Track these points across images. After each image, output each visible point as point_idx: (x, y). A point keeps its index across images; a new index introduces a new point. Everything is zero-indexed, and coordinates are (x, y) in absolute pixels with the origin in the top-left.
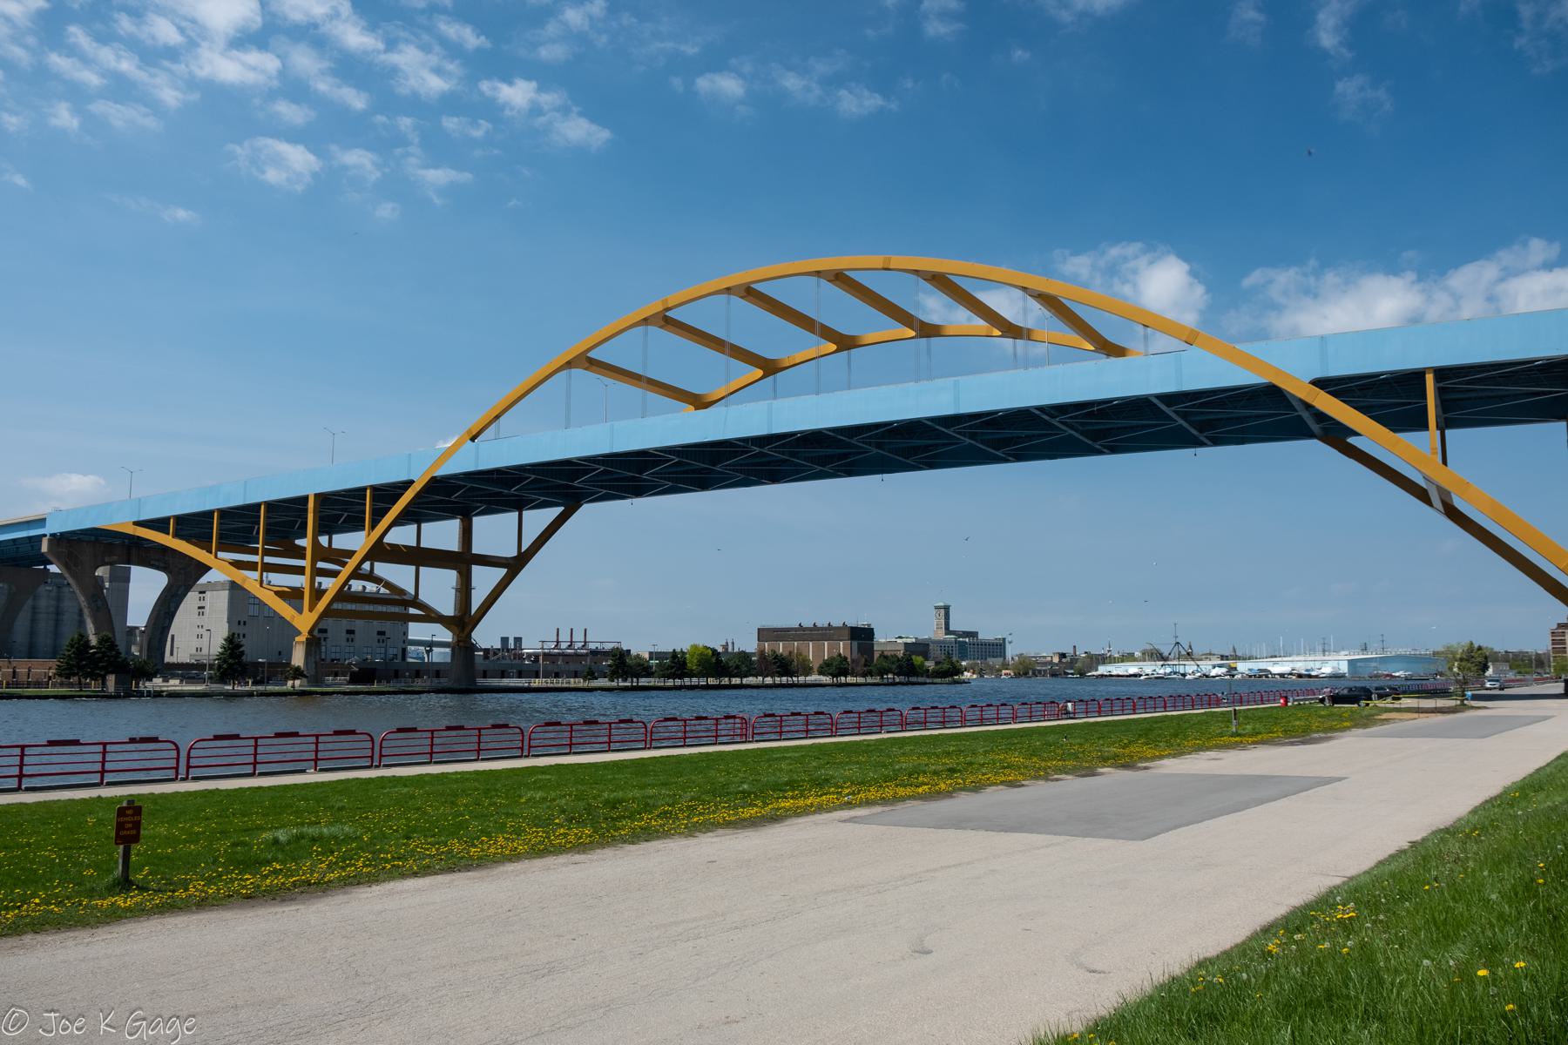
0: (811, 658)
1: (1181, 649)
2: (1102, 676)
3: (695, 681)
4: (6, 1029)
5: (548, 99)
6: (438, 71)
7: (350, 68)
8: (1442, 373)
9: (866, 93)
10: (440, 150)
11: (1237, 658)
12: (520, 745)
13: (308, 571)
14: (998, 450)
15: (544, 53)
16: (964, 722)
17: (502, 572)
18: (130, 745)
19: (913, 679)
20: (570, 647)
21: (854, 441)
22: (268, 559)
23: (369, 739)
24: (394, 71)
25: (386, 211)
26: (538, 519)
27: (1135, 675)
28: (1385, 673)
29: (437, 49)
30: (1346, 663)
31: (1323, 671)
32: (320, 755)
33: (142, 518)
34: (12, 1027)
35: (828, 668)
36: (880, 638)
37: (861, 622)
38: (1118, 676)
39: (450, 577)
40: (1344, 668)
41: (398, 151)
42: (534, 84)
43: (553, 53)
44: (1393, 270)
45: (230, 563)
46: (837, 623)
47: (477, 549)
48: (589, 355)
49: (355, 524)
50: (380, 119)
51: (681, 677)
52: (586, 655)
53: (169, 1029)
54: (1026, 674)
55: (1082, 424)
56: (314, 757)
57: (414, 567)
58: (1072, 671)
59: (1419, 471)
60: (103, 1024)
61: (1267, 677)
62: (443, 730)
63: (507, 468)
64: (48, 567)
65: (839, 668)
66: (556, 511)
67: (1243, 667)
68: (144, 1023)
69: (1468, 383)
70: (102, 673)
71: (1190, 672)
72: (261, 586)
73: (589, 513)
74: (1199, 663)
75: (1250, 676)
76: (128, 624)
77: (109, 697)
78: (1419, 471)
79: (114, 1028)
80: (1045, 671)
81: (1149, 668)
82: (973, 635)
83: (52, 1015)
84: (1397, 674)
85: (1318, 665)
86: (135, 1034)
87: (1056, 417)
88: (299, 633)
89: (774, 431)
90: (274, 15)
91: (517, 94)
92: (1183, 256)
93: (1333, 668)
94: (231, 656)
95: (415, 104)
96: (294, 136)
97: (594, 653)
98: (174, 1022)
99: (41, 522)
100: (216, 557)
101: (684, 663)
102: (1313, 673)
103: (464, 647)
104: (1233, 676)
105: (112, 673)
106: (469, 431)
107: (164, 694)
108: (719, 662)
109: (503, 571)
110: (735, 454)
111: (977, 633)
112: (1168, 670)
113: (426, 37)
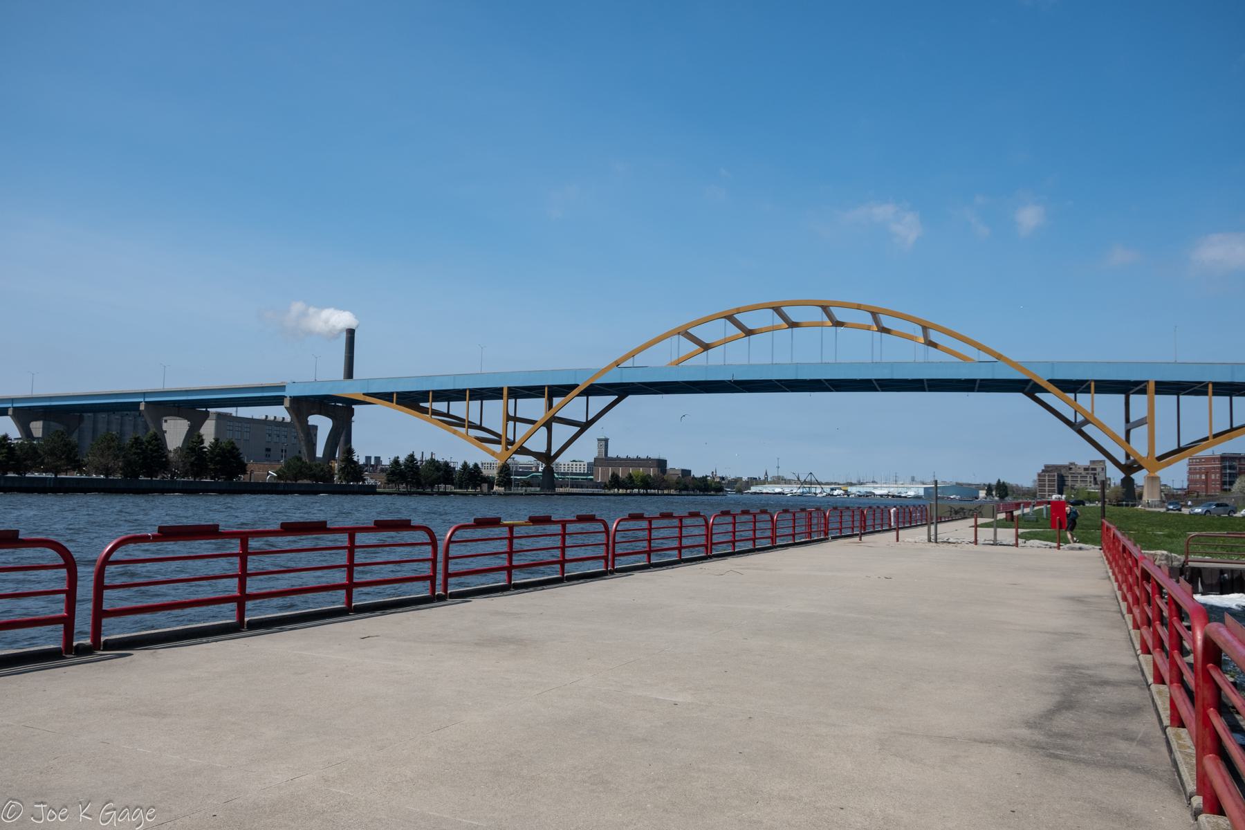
0: (620, 475)
1: (813, 478)
2: (755, 493)
4: (6, 818)
12: (57, 607)
17: (577, 429)
18: (722, 518)
23: (426, 538)
27: (779, 493)
31: (909, 493)
32: (570, 554)
33: (370, 392)
34: (10, 815)
36: (669, 466)
37: (662, 457)
38: (767, 493)
40: (921, 492)
60: (81, 814)
64: (208, 409)
68: (115, 812)
73: (631, 399)
74: (823, 486)
75: (860, 496)
79: (90, 816)
83: (42, 806)
84: (952, 497)
86: (107, 821)
89: (799, 378)
99: (282, 388)
101: (633, 481)
102: (903, 495)
103: (549, 471)
104: (848, 495)
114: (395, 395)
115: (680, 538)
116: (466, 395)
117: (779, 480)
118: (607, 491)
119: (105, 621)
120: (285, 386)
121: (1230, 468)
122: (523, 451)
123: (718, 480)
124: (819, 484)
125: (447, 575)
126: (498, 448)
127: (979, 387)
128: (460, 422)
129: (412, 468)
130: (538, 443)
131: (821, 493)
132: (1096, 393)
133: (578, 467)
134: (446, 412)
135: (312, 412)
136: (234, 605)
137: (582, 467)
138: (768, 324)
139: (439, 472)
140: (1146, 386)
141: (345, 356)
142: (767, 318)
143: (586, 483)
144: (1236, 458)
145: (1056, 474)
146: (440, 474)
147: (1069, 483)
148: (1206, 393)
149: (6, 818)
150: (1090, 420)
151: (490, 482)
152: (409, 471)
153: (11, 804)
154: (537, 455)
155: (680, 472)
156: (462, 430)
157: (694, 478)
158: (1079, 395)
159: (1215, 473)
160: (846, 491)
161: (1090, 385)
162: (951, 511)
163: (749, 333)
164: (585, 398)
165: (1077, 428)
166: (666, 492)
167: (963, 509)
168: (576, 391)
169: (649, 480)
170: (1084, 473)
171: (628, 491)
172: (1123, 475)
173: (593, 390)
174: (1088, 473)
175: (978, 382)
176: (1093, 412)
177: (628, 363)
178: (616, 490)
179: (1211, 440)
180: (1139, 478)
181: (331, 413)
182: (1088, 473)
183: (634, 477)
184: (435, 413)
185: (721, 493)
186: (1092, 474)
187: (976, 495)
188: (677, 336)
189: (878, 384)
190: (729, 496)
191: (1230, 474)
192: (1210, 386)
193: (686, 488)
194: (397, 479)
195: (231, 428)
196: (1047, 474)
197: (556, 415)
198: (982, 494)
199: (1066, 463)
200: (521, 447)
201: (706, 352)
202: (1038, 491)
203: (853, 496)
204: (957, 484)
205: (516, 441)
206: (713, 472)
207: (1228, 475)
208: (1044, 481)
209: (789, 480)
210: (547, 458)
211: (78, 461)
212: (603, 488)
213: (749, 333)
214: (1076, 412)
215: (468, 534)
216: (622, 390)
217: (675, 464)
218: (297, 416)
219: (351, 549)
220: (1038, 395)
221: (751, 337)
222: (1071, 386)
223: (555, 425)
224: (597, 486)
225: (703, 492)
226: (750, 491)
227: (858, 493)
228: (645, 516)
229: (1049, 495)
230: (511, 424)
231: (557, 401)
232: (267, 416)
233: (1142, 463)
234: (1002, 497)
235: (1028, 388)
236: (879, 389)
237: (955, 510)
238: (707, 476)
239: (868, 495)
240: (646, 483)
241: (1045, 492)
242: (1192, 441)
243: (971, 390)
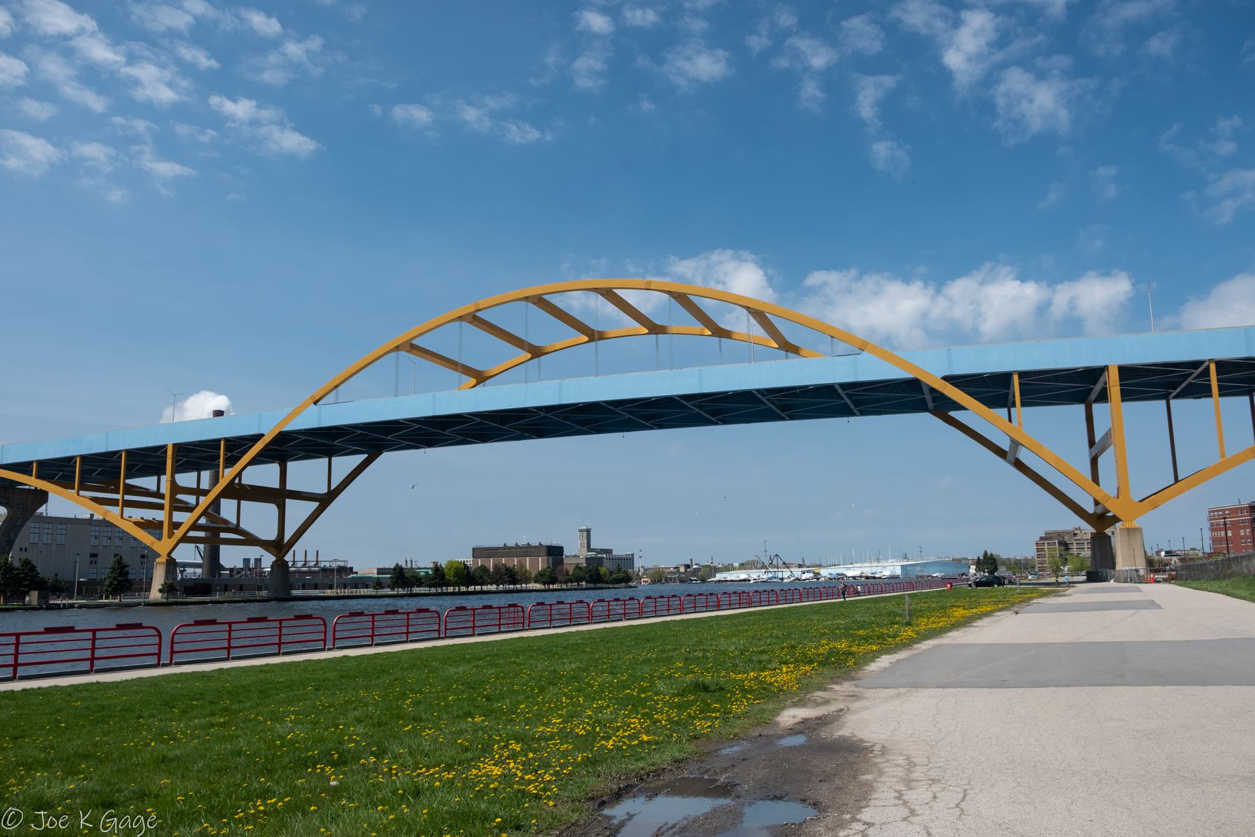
2: (719, 581)
3: (451, 589)
5: (267, 114)
6: (170, 85)
7: (92, 76)
8: (1022, 375)
9: (528, 129)
10: (168, 148)
11: (820, 566)
12: (155, 649)
13: (167, 507)
14: (713, 417)
15: (269, 77)
16: (590, 619)
17: (315, 505)
19: (599, 585)
20: (304, 565)
21: (617, 410)
22: (127, 497)
23: (322, 623)
24: (136, 82)
25: (117, 196)
26: (344, 464)
27: (744, 580)
28: (927, 574)
29: (174, 68)
30: (900, 567)
31: (884, 573)
35: (540, 578)
37: (555, 543)
38: (732, 581)
39: (272, 509)
40: (898, 571)
41: (135, 148)
42: (254, 103)
43: (273, 77)
44: (907, 279)
45: (90, 499)
46: (535, 543)
47: (289, 487)
48: (413, 342)
49: (159, 470)
50: (118, 120)
51: (441, 586)
52: (318, 572)
54: (660, 581)
55: (779, 401)
56: (227, 646)
57: (236, 501)
58: (695, 578)
59: (1008, 435)
60: (82, 821)
61: (843, 579)
62: (383, 614)
63: (345, 426)
65: (551, 578)
66: (360, 458)
67: (825, 572)
68: (116, 819)
69: (1034, 380)
70: (26, 590)
71: (786, 577)
72: (122, 517)
73: (388, 459)
75: (831, 579)
76: (221, 546)
77: (34, 609)
78: (1008, 435)
80: (675, 578)
81: (754, 575)
82: (609, 551)
83: (42, 813)
84: (935, 575)
85: (880, 569)
87: (766, 396)
88: (159, 556)
89: (563, 403)
90: (27, 26)
91: (241, 109)
92: (763, 264)
93: (891, 571)
94: (120, 574)
95: (149, 110)
96: (36, 130)
97: (325, 570)
98: (140, 818)
100: (78, 494)
101: (443, 576)
102: (877, 576)
103: (280, 565)
104: (818, 579)
105: (35, 589)
106: (313, 397)
107: (76, 606)
108: (468, 573)
109: (317, 504)
110: (524, 417)
111: (612, 550)
112: (770, 575)
113: (164, 58)
115: (408, 626)
116: (121, 462)
119: (336, 641)
125: (446, 629)
136: (89, 662)
145: (1056, 541)
153: (12, 811)
154: (265, 544)
159: (1244, 528)
195: (63, 532)
196: (1046, 542)
210: (279, 546)
215: (346, 620)
219: (94, 639)
228: (218, 621)
239: (841, 577)
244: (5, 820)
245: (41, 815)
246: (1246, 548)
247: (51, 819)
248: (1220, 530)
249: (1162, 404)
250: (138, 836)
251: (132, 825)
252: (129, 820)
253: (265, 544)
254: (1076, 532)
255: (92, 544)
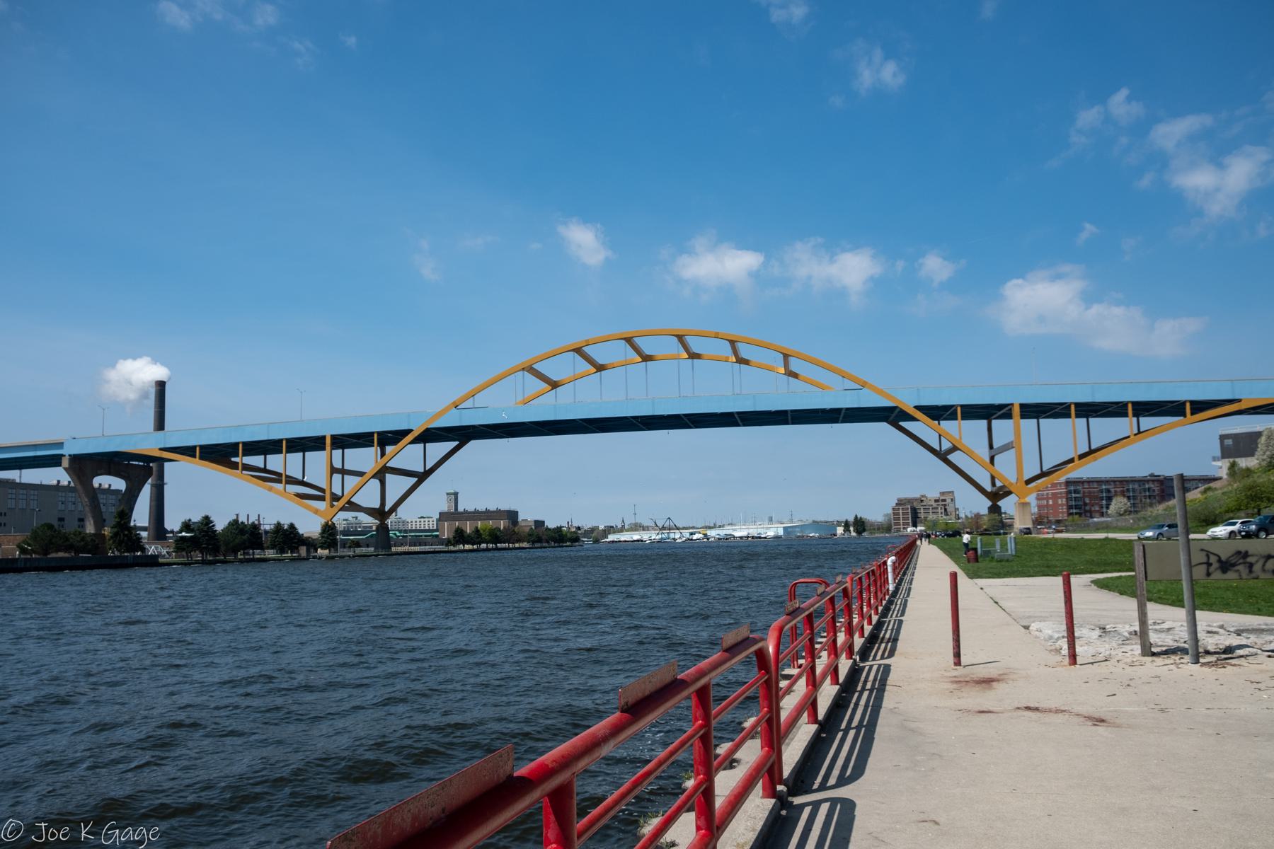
2: (613, 542)
4: (8, 838)
26: (437, 450)
27: (638, 541)
31: (768, 534)
36: (521, 518)
37: (513, 508)
38: (626, 541)
40: (781, 532)
53: (137, 837)
60: (83, 832)
66: (454, 444)
68: (117, 831)
70: (296, 545)
73: (474, 445)
74: (681, 531)
75: (719, 539)
83: (43, 824)
84: (811, 535)
98: (142, 830)
99: (60, 445)
101: (480, 535)
102: (762, 536)
103: (383, 529)
104: (708, 539)
109: (416, 479)
114: (198, 449)
116: (282, 447)
117: (636, 527)
118: (451, 548)
120: (63, 443)
121: (1076, 491)
122: (352, 506)
123: (573, 530)
124: (678, 529)
126: (321, 505)
127: (844, 417)
128: (276, 477)
129: (206, 531)
130: (369, 496)
131: (680, 538)
132: (962, 419)
133: (427, 523)
134: (263, 467)
135: (99, 472)
137: (431, 523)
138: (621, 359)
139: (244, 535)
140: (1011, 409)
141: (155, 411)
142: (620, 351)
143: (430, 541)
144: (1079, 482)
145: (909, 507)
146: (245, 537)
147: (922, 515)
148: (1068, 416)
149: (5, 836)
150: (959, 447)
151: (310, 544)
152: (204, 536)
153: (11, 822)
154: (371, 512)
155: (533, 524)
156: (280, 487)
157: (548, 529)
158: (941, 422)
159: (1061, 498)
160: (705, 535)
161: (956, 410)
162: (1209, 564)
163: (600, 368)
164: (423, 445)
165: (943, 456)
166: (517, 545)
167: (1246, 555)
168: (410, 437)
169: (498, 533)
170: (935, 505)
171: (475, 547)
172: (989, 503)
173: (429, 436)
174: (938, 505)
175: (843, 411)
176: (961, 438)
177: (468, 404)
178: (461, 546)
179: (1077, 462)
180: (1007, 505)
181: (122, 473)
182: (938, 505)
183: (481, 531)
184: (247, 467)
185: (577, 544)
186: (942, 505)
187: (834, 532)
188: (521, 372)
189: (739, 417)
190: (585, 546)
191: (1075, 498)
192: (1073, 407)
193: (539, 540)
194: (188, 547)
195: (36, 497)
197: (387, 465)
198: (840, 530)
199: (917, 496)
200: (349, 502)
201: (554, 390)
202: (893, 522)
203: (713, 539)
204: (814, 522)
205: (345, 494)
206: (568, 522)
207: (1073, 499)
208: (898, 514)
209: (648, 527)
210: (381, 513)
211: (217, 539)
212: (447, 545)
213: (600, 368)
214: (940, 436)
216: (463, 435)
217: (527, 515)
218: (79, 478)
220: (902, 423)
221: (603, 372)
222: (938, 413)
223: (389, 477)
224: (442, 542)
225: (558, 543)
226: (607, 540)
227: (718, 537)
229: (904, 528)
230: (338, 478)
231: (389, 449)
232: (59, 482)
233: (1012, 489)
234: (859, 532)
235: (893, 416)
236: (740, 423)
237: (1220, 560)
238: (561, 527)
240: (495, 537)
241: (900, 525)
242: (1054, 465)
243: (836, 421)
244: (7, 829)
245: (41, 826)
246: (1062, 513)
247: (52, 831)
248: (1043, 499)
249: (1035, 420)
250: (140, 848)
251: (134, 837)
252: (131, 832)
253: (371, 512)
254: (922, 499)
255: (59, 509)
